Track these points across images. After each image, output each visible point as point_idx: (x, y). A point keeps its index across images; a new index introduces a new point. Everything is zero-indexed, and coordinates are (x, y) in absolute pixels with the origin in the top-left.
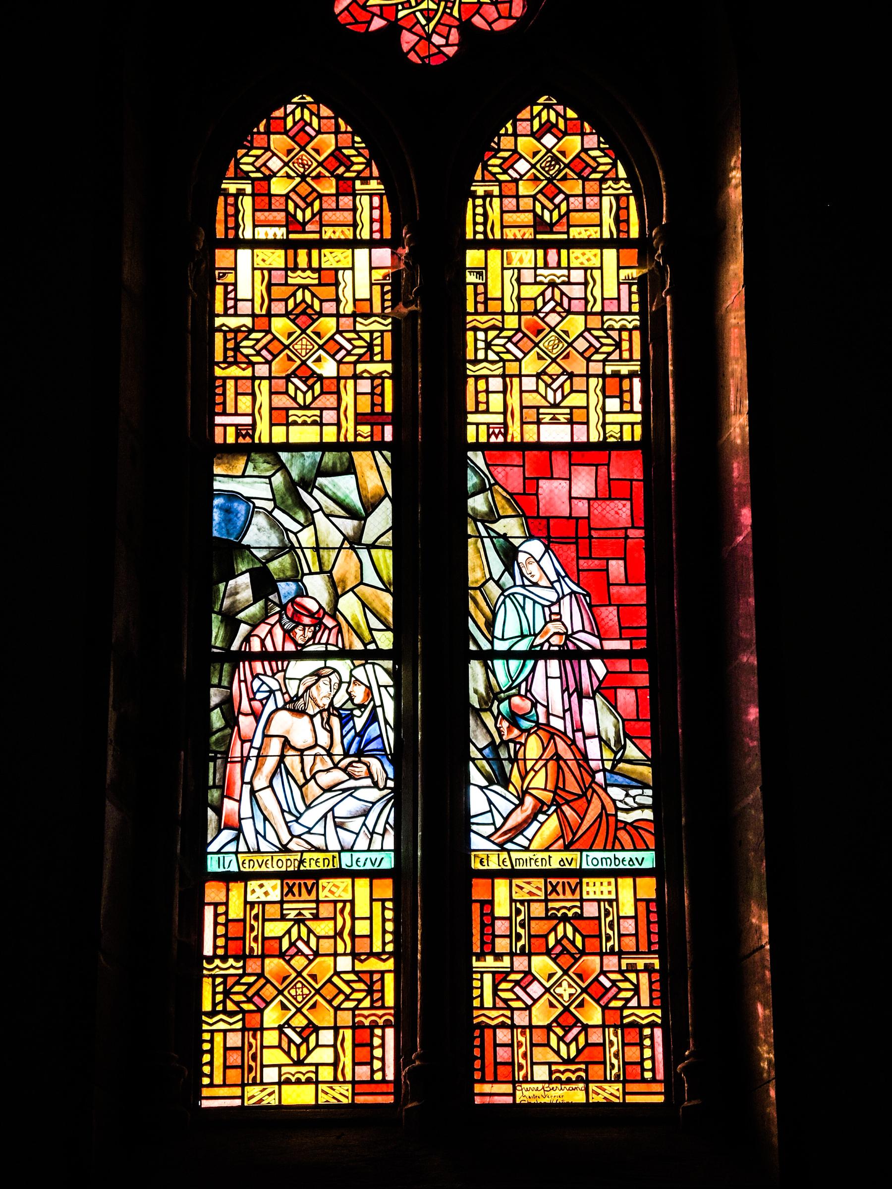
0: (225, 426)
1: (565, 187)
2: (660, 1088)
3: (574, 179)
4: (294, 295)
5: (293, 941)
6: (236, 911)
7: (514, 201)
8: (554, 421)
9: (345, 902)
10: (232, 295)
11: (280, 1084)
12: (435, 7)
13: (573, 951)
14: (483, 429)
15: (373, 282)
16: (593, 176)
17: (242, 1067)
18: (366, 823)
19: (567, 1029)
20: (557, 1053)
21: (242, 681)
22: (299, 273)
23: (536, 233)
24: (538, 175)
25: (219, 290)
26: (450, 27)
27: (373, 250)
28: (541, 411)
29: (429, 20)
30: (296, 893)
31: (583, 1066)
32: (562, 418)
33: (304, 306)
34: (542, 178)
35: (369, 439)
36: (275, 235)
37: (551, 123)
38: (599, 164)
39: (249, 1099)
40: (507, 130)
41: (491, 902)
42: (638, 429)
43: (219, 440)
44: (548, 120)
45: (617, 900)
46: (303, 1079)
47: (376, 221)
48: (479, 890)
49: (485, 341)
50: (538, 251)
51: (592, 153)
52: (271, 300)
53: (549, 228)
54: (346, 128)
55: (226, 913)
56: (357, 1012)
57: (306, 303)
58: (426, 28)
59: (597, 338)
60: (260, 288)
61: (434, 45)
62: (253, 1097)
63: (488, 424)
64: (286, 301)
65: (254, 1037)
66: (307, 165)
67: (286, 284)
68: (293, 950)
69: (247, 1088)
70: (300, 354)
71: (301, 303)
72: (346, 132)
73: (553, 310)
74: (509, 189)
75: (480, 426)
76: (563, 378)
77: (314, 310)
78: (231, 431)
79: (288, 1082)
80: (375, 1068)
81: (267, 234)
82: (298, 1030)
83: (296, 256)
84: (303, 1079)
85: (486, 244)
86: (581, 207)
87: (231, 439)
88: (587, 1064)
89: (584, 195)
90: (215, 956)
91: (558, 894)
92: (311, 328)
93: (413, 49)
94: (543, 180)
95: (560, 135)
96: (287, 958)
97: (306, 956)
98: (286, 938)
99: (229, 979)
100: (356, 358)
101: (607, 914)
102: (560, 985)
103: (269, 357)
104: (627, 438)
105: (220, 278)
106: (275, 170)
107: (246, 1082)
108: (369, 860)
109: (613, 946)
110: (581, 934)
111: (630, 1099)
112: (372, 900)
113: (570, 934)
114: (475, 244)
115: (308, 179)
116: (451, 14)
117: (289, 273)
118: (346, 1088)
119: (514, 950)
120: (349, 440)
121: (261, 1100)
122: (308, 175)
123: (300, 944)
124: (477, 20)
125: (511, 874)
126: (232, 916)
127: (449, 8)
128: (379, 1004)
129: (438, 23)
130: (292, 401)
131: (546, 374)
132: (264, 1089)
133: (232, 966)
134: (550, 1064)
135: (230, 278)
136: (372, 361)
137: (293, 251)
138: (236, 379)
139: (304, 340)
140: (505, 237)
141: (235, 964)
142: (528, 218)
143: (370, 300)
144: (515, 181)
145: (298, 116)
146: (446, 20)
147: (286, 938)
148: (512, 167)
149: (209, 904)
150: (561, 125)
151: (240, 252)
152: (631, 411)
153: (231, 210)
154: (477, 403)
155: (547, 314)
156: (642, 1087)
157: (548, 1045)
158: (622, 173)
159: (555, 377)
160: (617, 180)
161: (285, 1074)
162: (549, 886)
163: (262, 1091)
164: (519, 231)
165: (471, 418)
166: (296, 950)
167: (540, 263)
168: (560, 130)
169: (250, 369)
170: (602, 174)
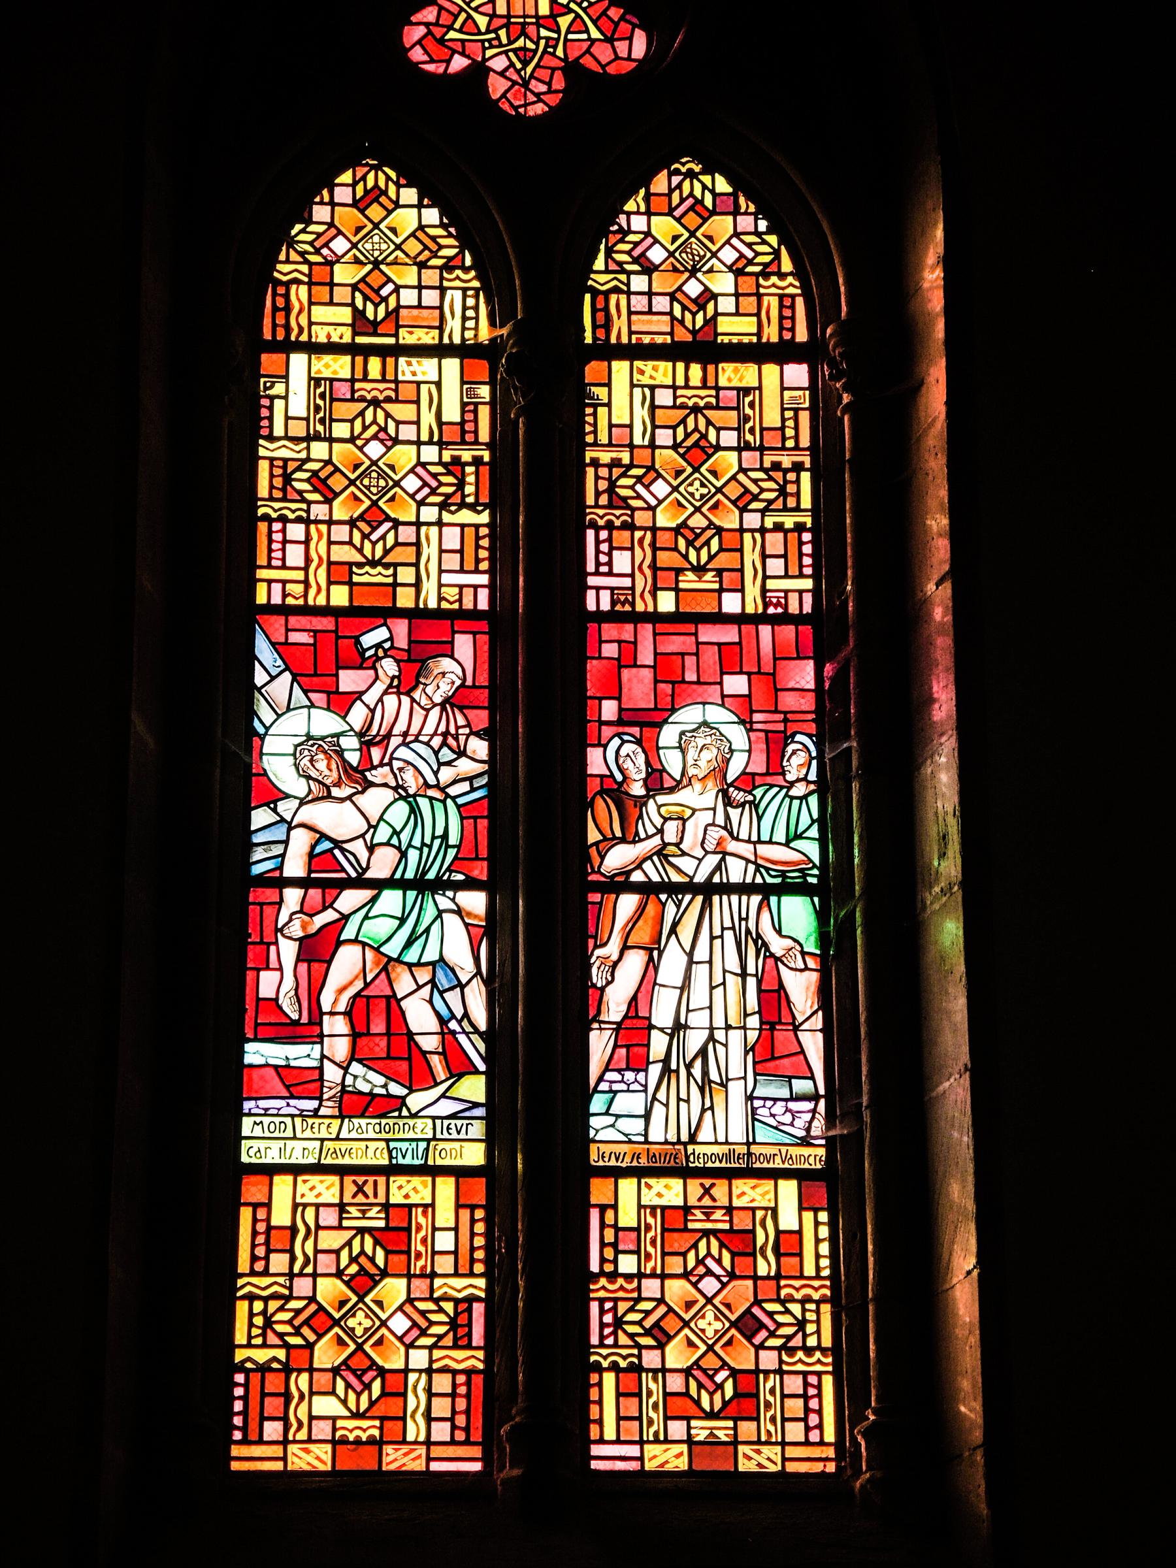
0: (270, 582)
2: (477, 1452)
3: (407, 264)
6: (628, 1217)
7: (645, 299)
9: (766, 1209)
12: (533, 46)
13: (373, 1271)
14: (276, 588)
15: (785, 406)
16: (750, 269)
17: (639, 1419)
19: (359, 1373)
21: (744, 919)
23: (355, 334)
24: (678, 266)
26: (553, 70)
27: (785, 367)
29: (525, 64)
30: (371, 1193)
31: (377, 1423)
35: (456, 606)
36: (329, 336)
37: (379, 188)
38: (441, 247)
40: (322, 198)
42: (808, 599)
43: (591, 606)
44: (376, 185)
45: (433, 1205)
47: (601, 326)
48: (600, 1190)
49: (609, 479)
51: (431, 231)
52: (655, 427)
53: (373, 327)
54: (748, 207)
55: (268, 1219)
58: (523, 73)
60: (641, 413)
61: (532, 92)
62: (655, 1457)
63: (612, 589)
65: (655, 1380)
66: (699, 255)
68: (701, 1270)
69: (646, 1447)
72: (746, 213)
73: (375, 437)
75: (479, 590)
76: (710, 533)
77: (709, 442)
78: (605, 597)
80: (812, 1424)
82: (359, 1373)
87: (605, 606)
88: (382, 1419)
89: (420, 287)
90: (602, 1273)
91: (367, 1197)
92: (706, 465)
93: (504, 95)
95: (706, 215)
96: (694, 1279)
97: (718, 1277)
99: (620, 1304)
104: (468, 604)
105: (266, 389)
106: (340, 254)
107: (645, 1438)
108: (613, 1155)
109: (425, 1267)
111: (435, 1466)
115: (383, 267)
116: (553, 54)
118: (324, 1450)
119: (643, 1270)
120: (790, 611)
122: (699, 270)
123: (710, 1262)
124: (587, 61)
126: (275, 1222)
128: (464, 1342)
129: (538, 66)
130: (682, 559)
131: (687, 527)
140: (313, 340)
142: (345, 315)
144: (331, 264)
145: (370, 183)
146: (548, 61)
148: (326, 245)
149: (247, 1204)
150: (708, 201)
151: (293, 357)
153: (281, 302)
154: (598, 564)
155: (368, 441)
156: (451, 1451)
157: (333, 1393)
158: (787, 265)
159: (698, 531)
160: (782, 276)
165: (262, 574)
166: (704, 1270)
167: (680, 381)
168: (706, 208)
170: (761, 267)
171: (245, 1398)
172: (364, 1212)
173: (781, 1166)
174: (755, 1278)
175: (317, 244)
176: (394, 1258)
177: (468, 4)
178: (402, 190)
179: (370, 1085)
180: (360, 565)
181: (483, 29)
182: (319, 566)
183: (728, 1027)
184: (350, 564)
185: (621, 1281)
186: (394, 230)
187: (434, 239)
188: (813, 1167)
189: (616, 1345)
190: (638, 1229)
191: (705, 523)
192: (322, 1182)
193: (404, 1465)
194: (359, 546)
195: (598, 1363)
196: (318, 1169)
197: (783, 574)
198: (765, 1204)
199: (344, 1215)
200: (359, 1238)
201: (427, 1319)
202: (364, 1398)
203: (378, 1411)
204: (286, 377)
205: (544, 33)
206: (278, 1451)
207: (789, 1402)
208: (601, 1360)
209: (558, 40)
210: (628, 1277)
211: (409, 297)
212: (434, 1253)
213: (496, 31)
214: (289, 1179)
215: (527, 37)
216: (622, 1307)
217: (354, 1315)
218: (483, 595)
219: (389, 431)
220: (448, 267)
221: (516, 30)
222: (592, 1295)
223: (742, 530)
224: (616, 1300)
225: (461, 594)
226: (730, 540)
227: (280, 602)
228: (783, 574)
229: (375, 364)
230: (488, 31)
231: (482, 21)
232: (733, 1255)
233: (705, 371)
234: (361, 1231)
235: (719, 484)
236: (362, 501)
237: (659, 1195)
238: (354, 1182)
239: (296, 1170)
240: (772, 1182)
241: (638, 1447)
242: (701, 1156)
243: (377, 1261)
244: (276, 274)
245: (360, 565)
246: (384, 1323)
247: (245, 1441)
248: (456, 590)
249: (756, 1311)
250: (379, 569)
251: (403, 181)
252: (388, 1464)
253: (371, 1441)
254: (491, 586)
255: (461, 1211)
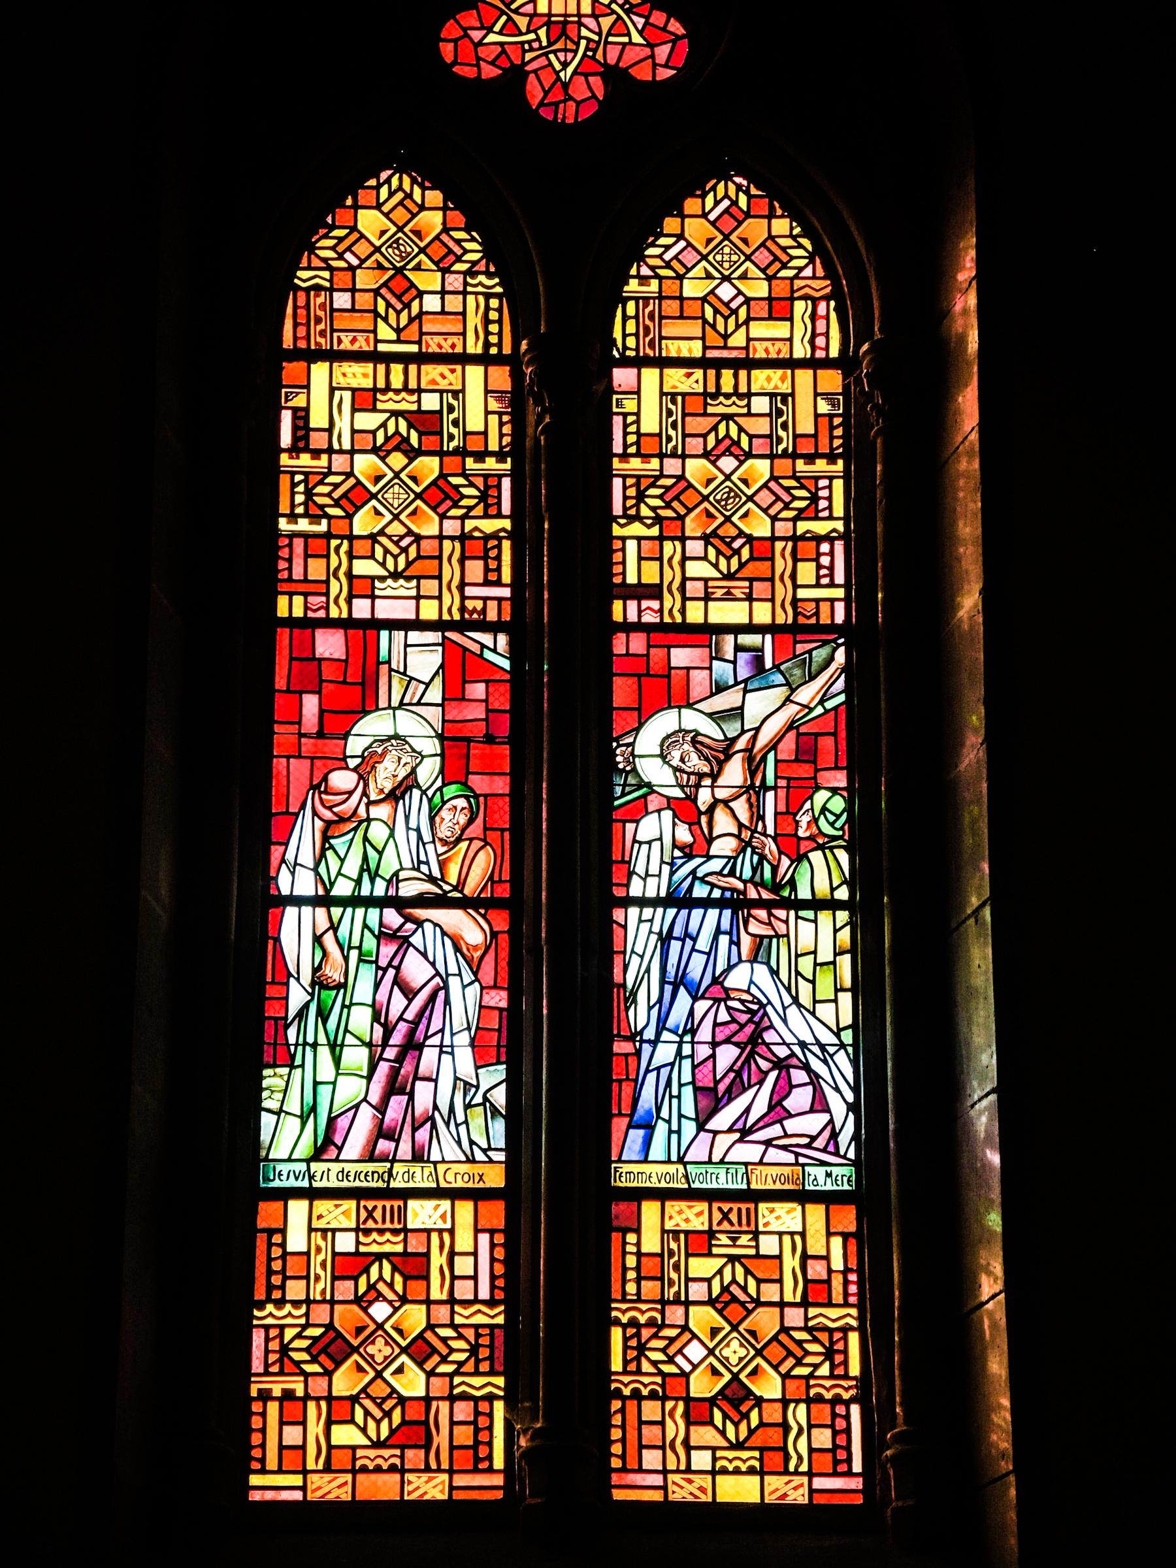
1: (418, 279)
4: (715, 428)
5: (372, 1282)
8: (729, 597)
10: (633, 428)
11: (714, 1473)
18: (667, 1125)
19: (379, 1401)
20: (723, 1433)
22: (391, 394)
25: (617, 421)
28: (711, 584)
31: (757, 1454)
32: (738, 593)
33: (727, 442)
34: (717, 275)
39: (313, 1491)
41: (283, 1231)
46: (744, 1468)
48: (267, 1213)
50: (709, 371)
55: (283, 1245)
56: (812, 1382)
57: (731, 438)
59: (787, 490)
62: (319, 1488)
64: (704, 436)
67: (705, 414)
70: (392, 505)
71: (724, 438)
74: (343, 279)
79: (724, 1471)
81: (690, 350)
82: (379, 1401)
83: (718, 377)
84: (744, 1468)
85: (639, 362)
86: (348, 306)
88: (761, 1450)
89: (443, 293)
91: (732, 1224)
94: (389, 269)
97: (390, 1303)
98: (717, 1280)
100: (795, 513)
101: (319, 1250)
102: (387, 1343)
103: (682, 511)
104: (825, 619)
108: (292, 1174)
110: (402, 1274)
112: (829, 1234)
113: (740, 1278)
114: (625, 362)
116: (524, 51)
117: (379, 396)
121: (785, 1495)
125: (312, 1194)
126: (290, 1248)
127: (530, 46)
132: (790, 1481)
133: (271, 1315)
134: (714, 1449)
135: (300, 401)
136: (816, 518)
137: (714, 371)
138: (639, 539)
139: (397, 487)
141: (619, 1315)
143: (485, 433)
147: (717, 1280)
151: (645, 371)
152: (832, 585)
161: (361, 1458)
162: (362, 1211)
163: (787, 1483)
164: (773, 345)
165: (840, 593)
169: (657, 528)
171: (623, 1427)
172: (734, 1240)
173: (658, 1185)
174: (428, 1302)
175: (340, 249)
176: (412, 1284)
177: (508, 6)
178: (427, 192)
179: (364, 1105)
180: (382, 579)
181: (524, 30)
182: (671, 583)
183: (315, 1045)
184: (372, 578)
185: (288, 1307)
186: (745, 241)
187: (784, 249)
188: (454, 1185)
189: (639, 1372)
190: (661, 1255)
191: (403, 531)
192: (690, 1207)
193: (426, 1493)
194: (388, 556)
195: (618, 1390)
196: (690, 1195)
197: (437, 581)
198: (440, 1225)
199: (713, 1242)
200: (729, 1266)
201: (448, 1346)
202: (743, 1427)
203: (756, 1441)
204: (307, 387)
205: (542, 32)
206: (657, 1480)
207: (646, 1430)
208: (642, 1388)
209: (598, 43)
210: (296, 1304)
211: (432, 303)
212: (688, 1280)
213: (535, 31)
214: (304, 1204)
215: (567, 37)
216: (289, 1333)
217: (373, 1343)
218: (840, 608)
219: (742, 445)
220: (471, 273)
221: (556, 31)
222: (255, 1322)
223: (441, 537)
224: (282, 1328)
225: (818, 607)
226: (428, 547)
227: (301, 615)
228: (437, 581)
229: (727, 375)
230: (528, 32)
231: (522, 22)
232: (406, 1279)
233: (736, 376)
234: (732, 1259)
235: (749, 492)
236: (716, 518)
237: (687, 1220)
238: (720, 1209)
239: (663, 1195)
240: (659, 1204)
241: (301, 1476)
242: (839, 1178)
243: (749, 1291)
244: (296, 281)
245: (382, 579)
246: (711, 1352)
247: (624, 1470)
248: (813, 605)
249: (429, 1335)
250: (401, 582)
251: (427, 184)
252: (313, 1491)
253: (392, 1469)
254: (847, 600)
255: (480, 1236)
